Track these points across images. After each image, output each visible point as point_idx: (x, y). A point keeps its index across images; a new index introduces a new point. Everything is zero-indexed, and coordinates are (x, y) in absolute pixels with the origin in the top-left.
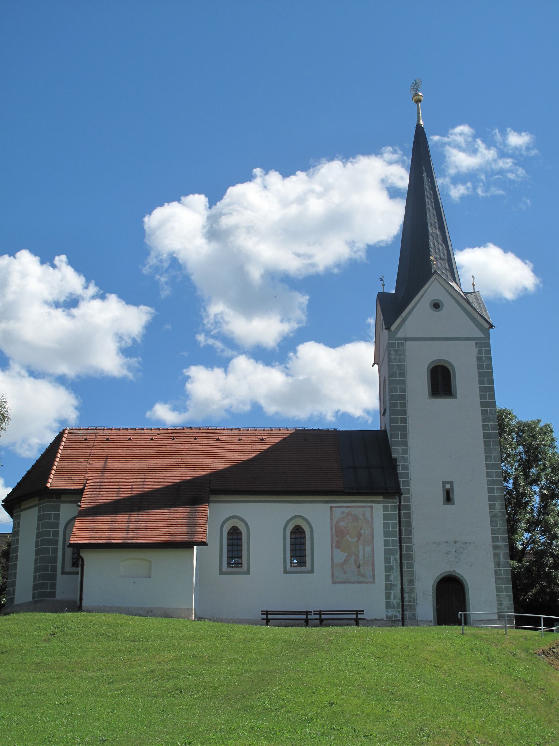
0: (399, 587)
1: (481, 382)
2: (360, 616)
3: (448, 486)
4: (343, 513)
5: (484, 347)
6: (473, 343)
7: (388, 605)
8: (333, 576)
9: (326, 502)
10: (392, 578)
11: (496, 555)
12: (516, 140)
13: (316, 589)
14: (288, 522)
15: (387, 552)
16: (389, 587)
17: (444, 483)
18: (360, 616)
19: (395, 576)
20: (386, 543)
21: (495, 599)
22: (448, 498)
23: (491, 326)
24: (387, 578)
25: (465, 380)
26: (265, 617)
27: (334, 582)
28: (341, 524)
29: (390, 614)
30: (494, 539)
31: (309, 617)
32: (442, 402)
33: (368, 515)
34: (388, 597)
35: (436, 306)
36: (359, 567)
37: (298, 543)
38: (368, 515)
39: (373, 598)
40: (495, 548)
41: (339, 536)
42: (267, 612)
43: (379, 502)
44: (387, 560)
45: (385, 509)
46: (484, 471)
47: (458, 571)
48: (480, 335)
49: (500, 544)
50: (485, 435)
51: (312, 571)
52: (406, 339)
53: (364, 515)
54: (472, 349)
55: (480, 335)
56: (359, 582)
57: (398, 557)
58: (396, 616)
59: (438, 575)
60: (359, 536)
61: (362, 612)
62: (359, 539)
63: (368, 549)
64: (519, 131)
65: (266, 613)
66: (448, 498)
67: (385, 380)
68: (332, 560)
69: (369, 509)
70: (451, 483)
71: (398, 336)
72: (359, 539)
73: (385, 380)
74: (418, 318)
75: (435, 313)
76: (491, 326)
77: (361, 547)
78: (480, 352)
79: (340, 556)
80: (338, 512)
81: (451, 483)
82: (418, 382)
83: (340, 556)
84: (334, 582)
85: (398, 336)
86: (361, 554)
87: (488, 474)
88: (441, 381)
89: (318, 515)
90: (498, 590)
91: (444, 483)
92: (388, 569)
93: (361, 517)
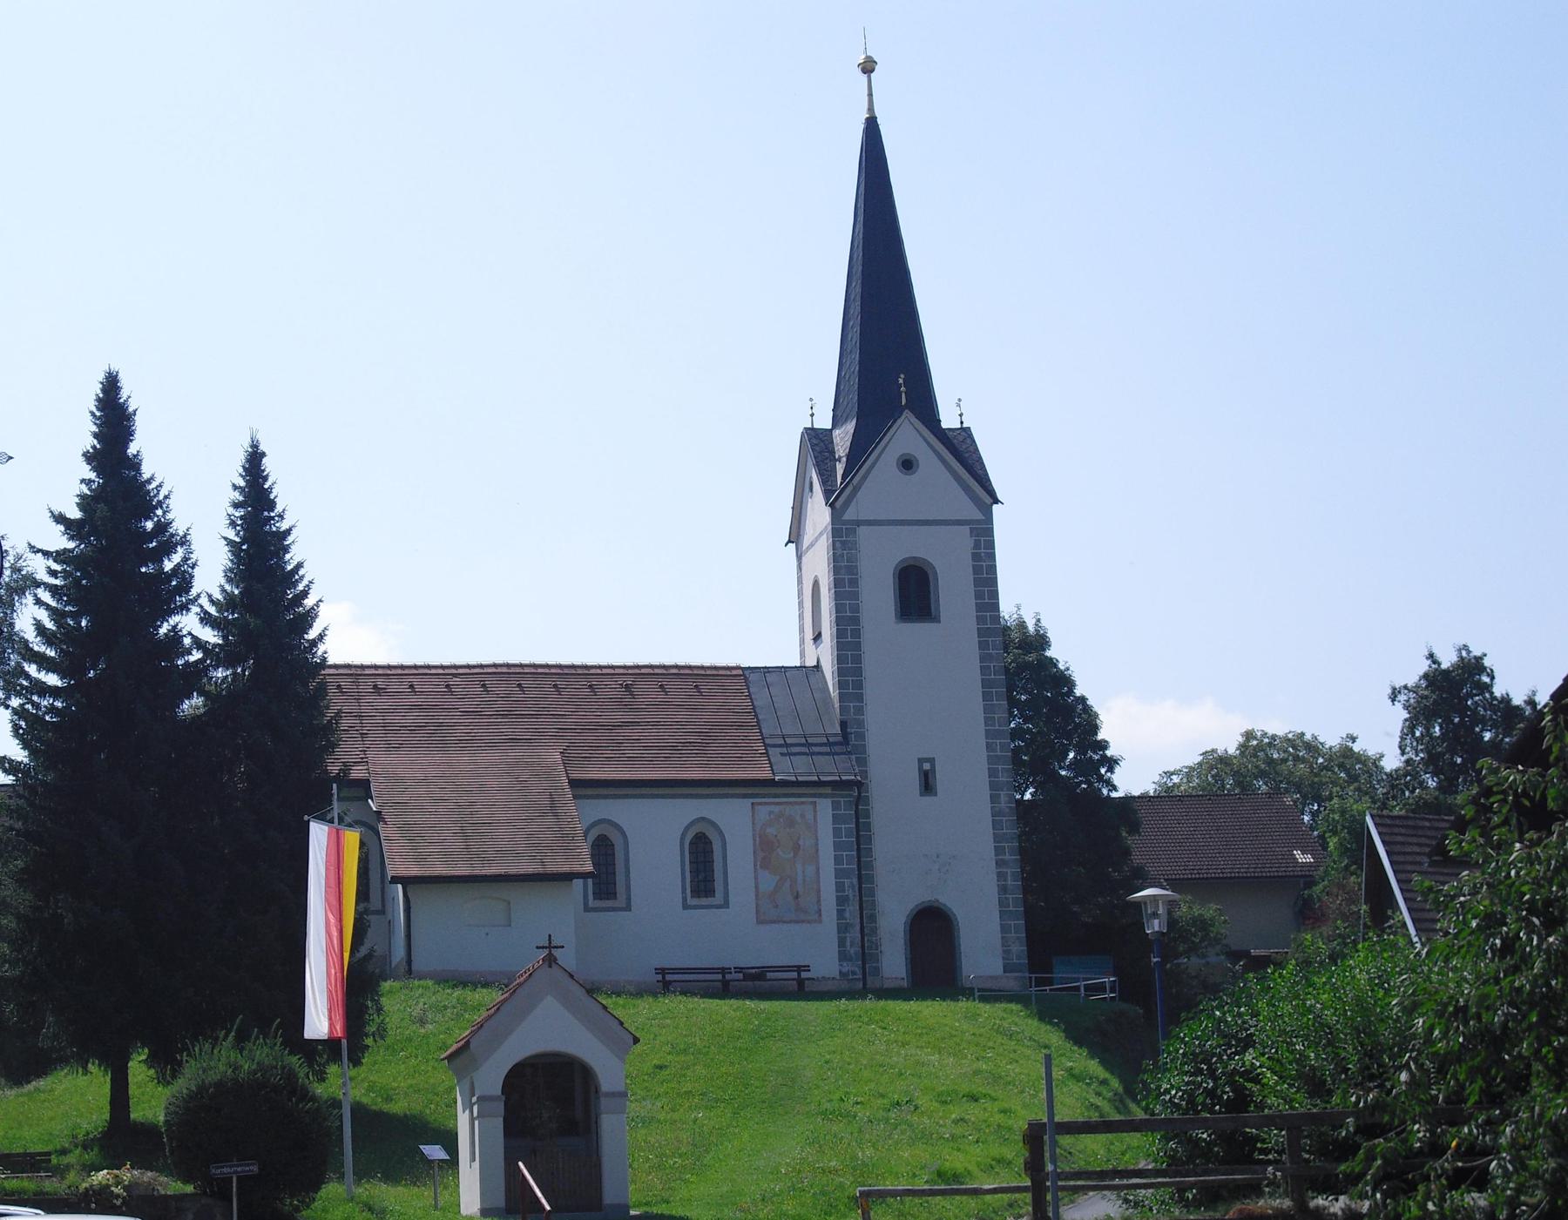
0: (858, 928)
1: (978, 595)
2: (804, 975)
3: (927, 766)
4: (770, 813)
5: (983, 535)
6: (966, 529)
7: (843, 956)
8: (757, 912)
9: (745, 796)
10: (847, 915)
11: (1001, 876)
12: (192, 705)
13: (735, 932)
14: (687, 828)
15: (839, 874)
16: (843, 929)
17: (921, 761)
18: (804, 975)
19: (852, 909)
20: (838, 860)
21: (999, 942)
22: (927, 784)
23: (996, 501)
24: (840, 913)
25: (953, 592)
26: (660, 977)
27: (760, 922)
28: (769, 830)
29: (845, 970)
30: (999, 851)
31: (728, 977)
32: (918, 630)
33: (810, 816)
34: (841, 943)
35: (907, 464)
36: (797, 897)
37: (701, 864)
38: (810, 816)
39: (820, 952)
40: (999, 863)
41: (765, 849)
42: (663, 970)
43: (826, 796)
44: (840, 887)
45: (835, 806)
46: (982, 741)
47: (943, 900)
48: (979, 516)
49: (1007, 857)
50: (985, 684)
51: (726, 904)
52: (859, 523)
53: (803, 816)
54: (962, 540)
55: (979, 516)
56: (797, 922)
57: (855, 881)
58: (854, 973)
59: (911, 906)
60: (796, 848)
61: (807, 968)
62: (796, 854)
63: (810, 869)
64: (195, 719)
65: (662, 971)
66: (927, 784)
67: (816, 584)
68: (757, 887)
69: (811, 807)
70: (932, 761)
71: (846, 517)
72: (796, 854)
73: (816, 584)
74: (882, 486)
75: (915, 478)
76: (996, 501)
77: (799, 867)
78: (977, 545)
79: (768, 881)
80: (763, 812)
81: (932, 761)
82: (879, 595)
83: (768, 881)
84: (760, 922)
85: (846, 517)
86: (800, 878)
87: (988, 746)
88: (915, 592)
89: (735, 821)
90: (1004, 929)
91: (921, 761)
92: (842, 901)
93: (798, 818)
